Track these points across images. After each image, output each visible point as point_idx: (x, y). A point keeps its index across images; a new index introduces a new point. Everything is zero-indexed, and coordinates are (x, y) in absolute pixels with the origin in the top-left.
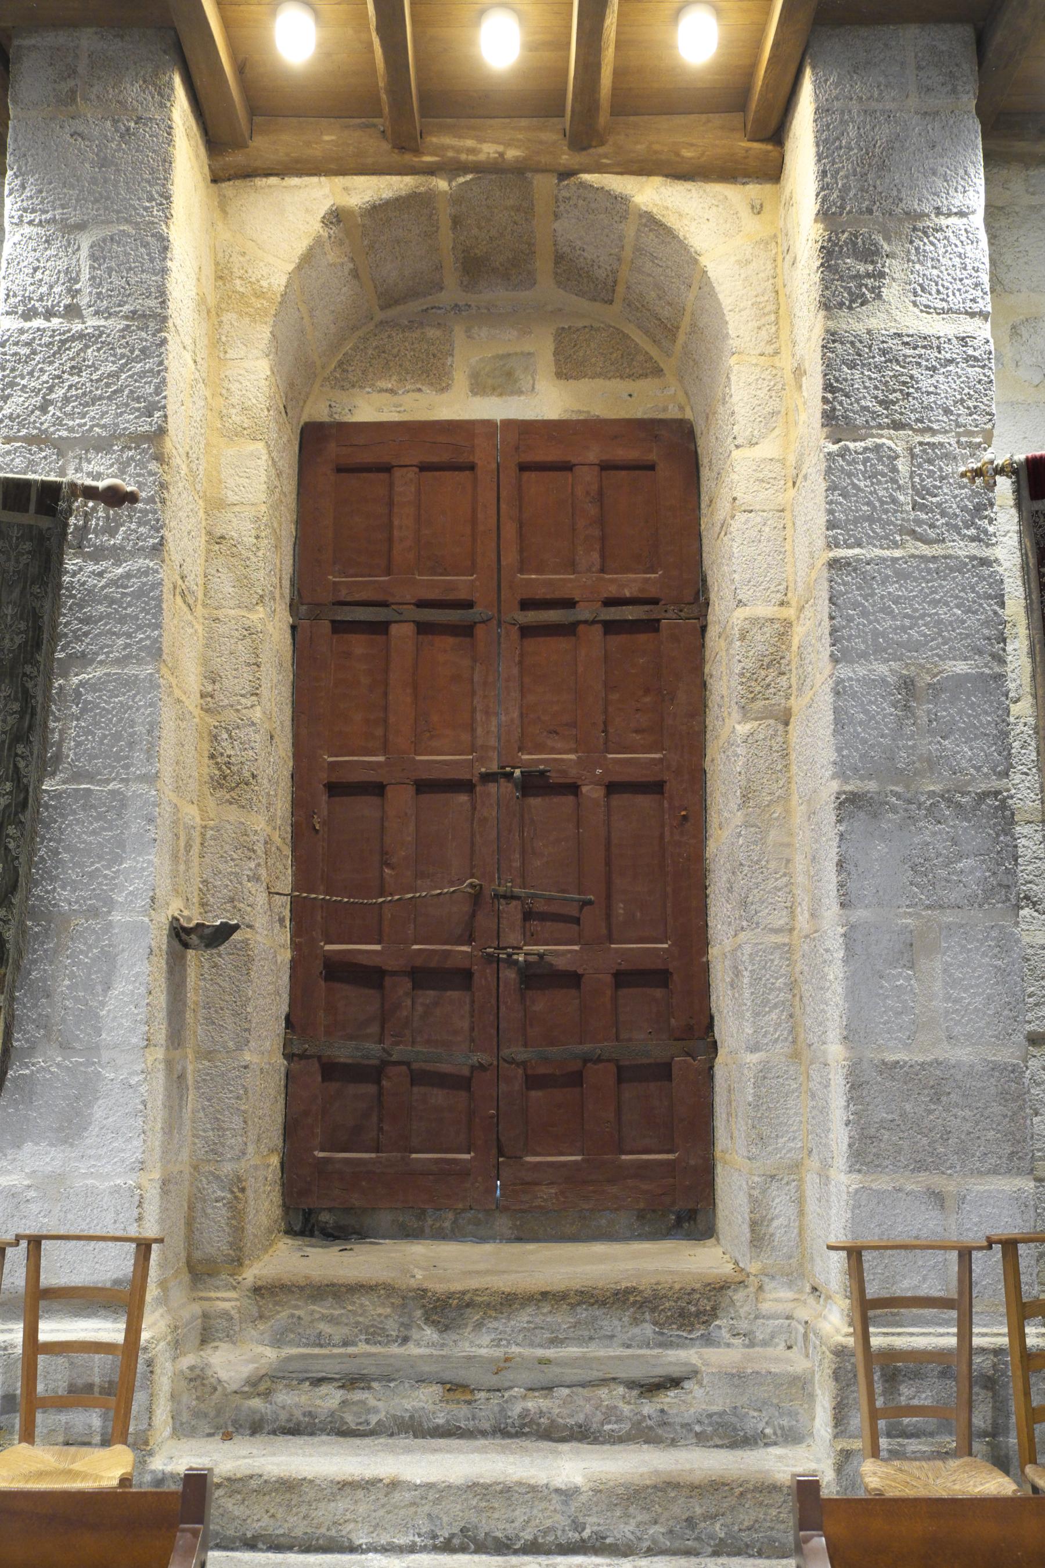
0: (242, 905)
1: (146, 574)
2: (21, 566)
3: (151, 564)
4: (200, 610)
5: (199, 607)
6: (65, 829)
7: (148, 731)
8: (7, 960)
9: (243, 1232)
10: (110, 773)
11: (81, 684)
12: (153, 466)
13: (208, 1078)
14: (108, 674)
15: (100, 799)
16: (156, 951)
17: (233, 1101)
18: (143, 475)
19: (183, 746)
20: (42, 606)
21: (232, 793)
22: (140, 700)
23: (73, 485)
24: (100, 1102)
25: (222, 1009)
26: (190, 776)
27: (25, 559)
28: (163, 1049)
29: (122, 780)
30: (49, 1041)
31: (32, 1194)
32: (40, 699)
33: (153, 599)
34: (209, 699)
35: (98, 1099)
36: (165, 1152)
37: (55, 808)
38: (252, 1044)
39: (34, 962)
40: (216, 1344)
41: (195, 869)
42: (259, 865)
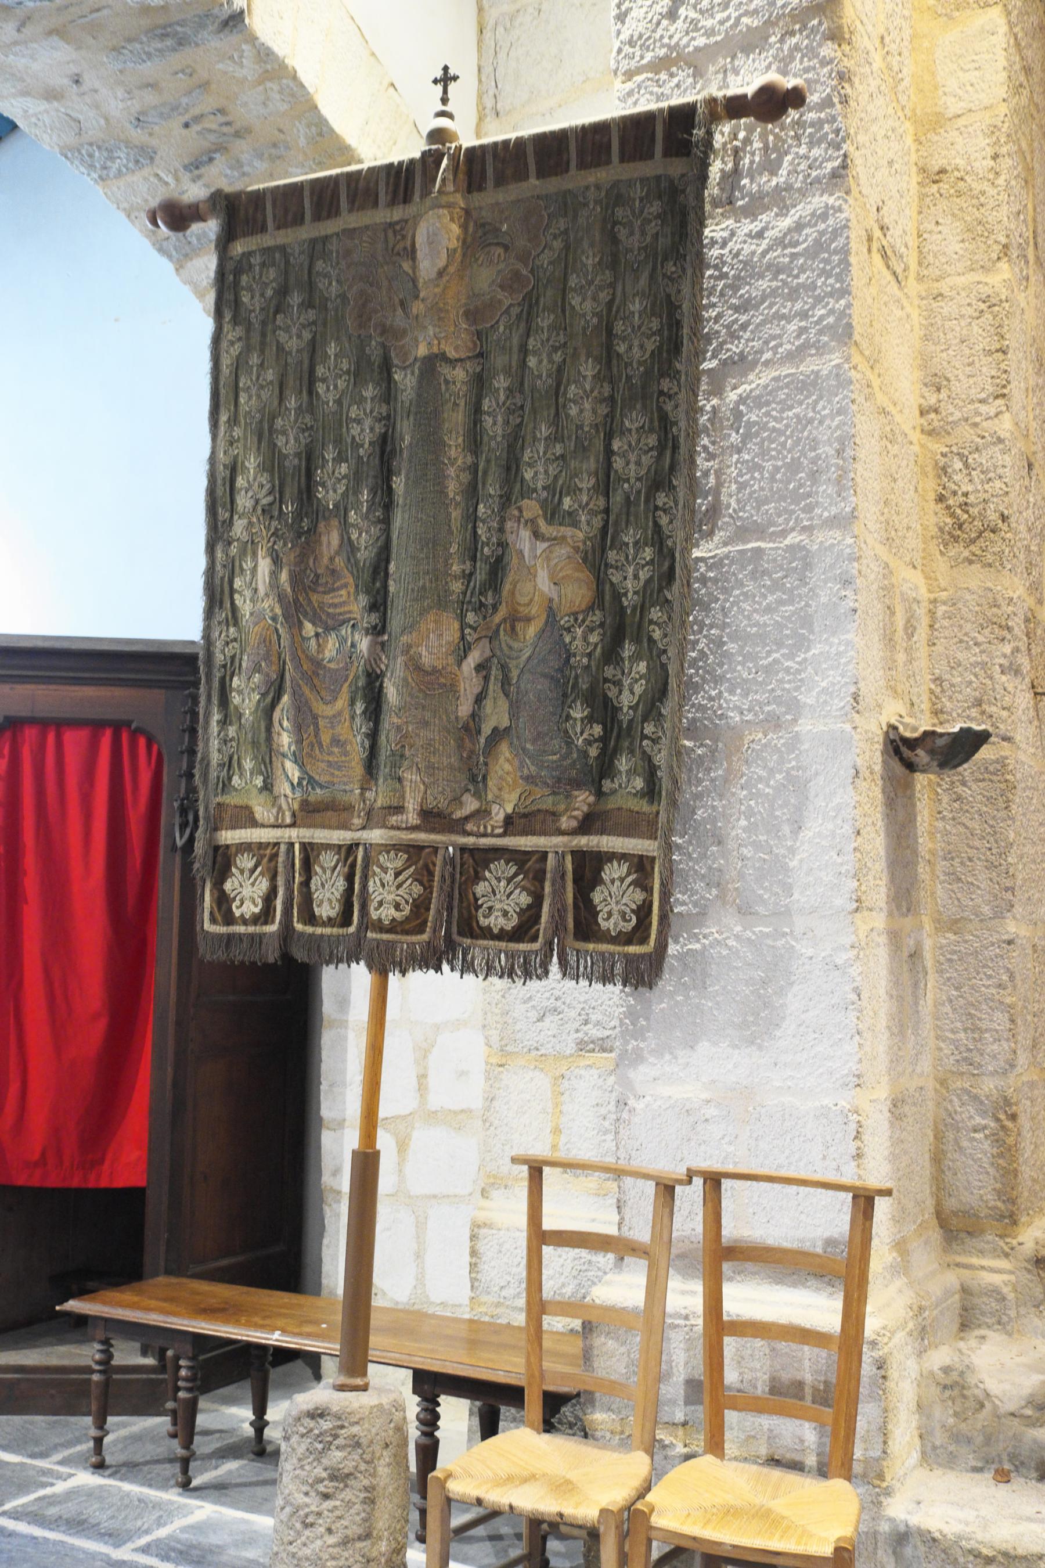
0: (994, 709)
1: (824, 217)
2: (648, 239)
3: (831, 201)
4: (912, 286)
5: (912, 281)
6: (730, 609)
7: (838, 452)
8: (660, 792)
9: (1016, 1176)
10: (787, 521)
11: (742, 400)
12: (828, 50)
13: (955, 957)
14: (776, 379)
15: (775, 560)
16: (864, 772)
17: (994, 991)
18: (814, 68)
19: (895, 480)
20: (679, 291)
21: (973, 548)
22: (824, 408)
23: (712, 101)
24: (795, 988)
25: (970, 860)
26: (908, 528)
27: (652, 228)
28: (883, 916)
29: (804, 529)
30: (724, 903)
31: (711, 1111)
32: (683, 424)
33: (836, 252)
34: (933, 415)
35: (792, 984)
36: (895, 1061)
37: (715, 580)
38: (1018, 910)
39: (698, 796)
40: (982, 1332)
41: (922, 662)
42: (1017, 650)
